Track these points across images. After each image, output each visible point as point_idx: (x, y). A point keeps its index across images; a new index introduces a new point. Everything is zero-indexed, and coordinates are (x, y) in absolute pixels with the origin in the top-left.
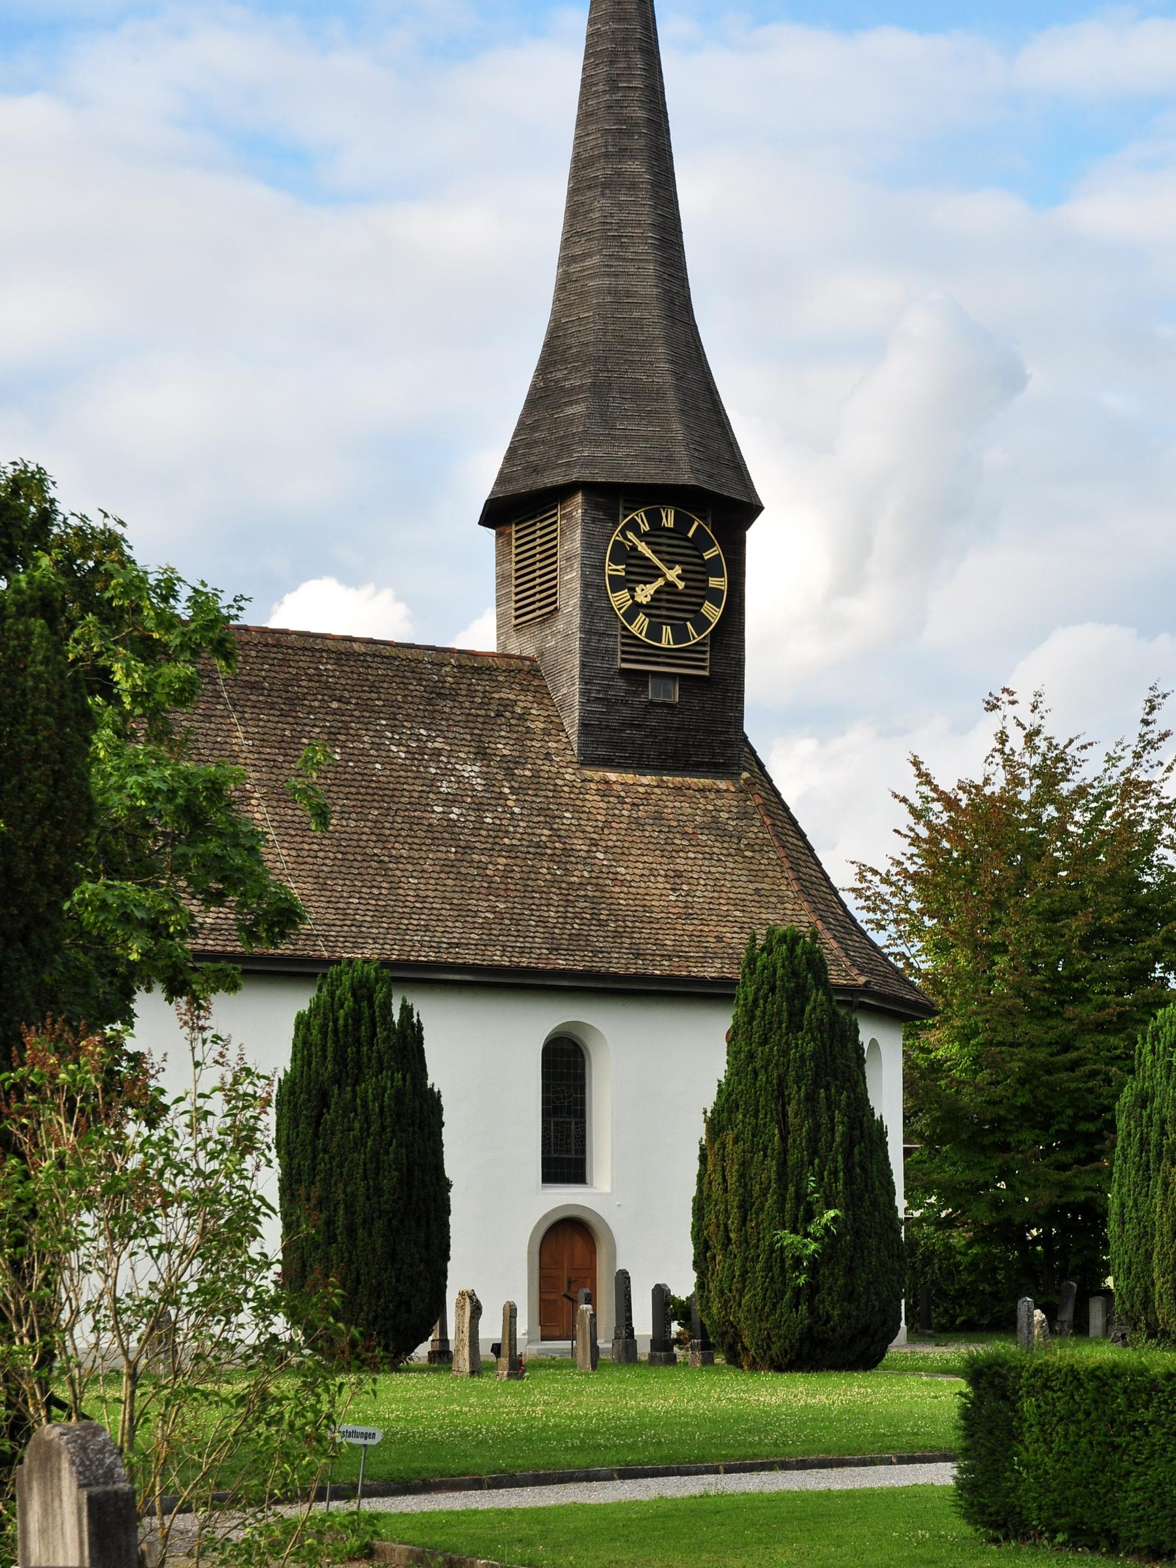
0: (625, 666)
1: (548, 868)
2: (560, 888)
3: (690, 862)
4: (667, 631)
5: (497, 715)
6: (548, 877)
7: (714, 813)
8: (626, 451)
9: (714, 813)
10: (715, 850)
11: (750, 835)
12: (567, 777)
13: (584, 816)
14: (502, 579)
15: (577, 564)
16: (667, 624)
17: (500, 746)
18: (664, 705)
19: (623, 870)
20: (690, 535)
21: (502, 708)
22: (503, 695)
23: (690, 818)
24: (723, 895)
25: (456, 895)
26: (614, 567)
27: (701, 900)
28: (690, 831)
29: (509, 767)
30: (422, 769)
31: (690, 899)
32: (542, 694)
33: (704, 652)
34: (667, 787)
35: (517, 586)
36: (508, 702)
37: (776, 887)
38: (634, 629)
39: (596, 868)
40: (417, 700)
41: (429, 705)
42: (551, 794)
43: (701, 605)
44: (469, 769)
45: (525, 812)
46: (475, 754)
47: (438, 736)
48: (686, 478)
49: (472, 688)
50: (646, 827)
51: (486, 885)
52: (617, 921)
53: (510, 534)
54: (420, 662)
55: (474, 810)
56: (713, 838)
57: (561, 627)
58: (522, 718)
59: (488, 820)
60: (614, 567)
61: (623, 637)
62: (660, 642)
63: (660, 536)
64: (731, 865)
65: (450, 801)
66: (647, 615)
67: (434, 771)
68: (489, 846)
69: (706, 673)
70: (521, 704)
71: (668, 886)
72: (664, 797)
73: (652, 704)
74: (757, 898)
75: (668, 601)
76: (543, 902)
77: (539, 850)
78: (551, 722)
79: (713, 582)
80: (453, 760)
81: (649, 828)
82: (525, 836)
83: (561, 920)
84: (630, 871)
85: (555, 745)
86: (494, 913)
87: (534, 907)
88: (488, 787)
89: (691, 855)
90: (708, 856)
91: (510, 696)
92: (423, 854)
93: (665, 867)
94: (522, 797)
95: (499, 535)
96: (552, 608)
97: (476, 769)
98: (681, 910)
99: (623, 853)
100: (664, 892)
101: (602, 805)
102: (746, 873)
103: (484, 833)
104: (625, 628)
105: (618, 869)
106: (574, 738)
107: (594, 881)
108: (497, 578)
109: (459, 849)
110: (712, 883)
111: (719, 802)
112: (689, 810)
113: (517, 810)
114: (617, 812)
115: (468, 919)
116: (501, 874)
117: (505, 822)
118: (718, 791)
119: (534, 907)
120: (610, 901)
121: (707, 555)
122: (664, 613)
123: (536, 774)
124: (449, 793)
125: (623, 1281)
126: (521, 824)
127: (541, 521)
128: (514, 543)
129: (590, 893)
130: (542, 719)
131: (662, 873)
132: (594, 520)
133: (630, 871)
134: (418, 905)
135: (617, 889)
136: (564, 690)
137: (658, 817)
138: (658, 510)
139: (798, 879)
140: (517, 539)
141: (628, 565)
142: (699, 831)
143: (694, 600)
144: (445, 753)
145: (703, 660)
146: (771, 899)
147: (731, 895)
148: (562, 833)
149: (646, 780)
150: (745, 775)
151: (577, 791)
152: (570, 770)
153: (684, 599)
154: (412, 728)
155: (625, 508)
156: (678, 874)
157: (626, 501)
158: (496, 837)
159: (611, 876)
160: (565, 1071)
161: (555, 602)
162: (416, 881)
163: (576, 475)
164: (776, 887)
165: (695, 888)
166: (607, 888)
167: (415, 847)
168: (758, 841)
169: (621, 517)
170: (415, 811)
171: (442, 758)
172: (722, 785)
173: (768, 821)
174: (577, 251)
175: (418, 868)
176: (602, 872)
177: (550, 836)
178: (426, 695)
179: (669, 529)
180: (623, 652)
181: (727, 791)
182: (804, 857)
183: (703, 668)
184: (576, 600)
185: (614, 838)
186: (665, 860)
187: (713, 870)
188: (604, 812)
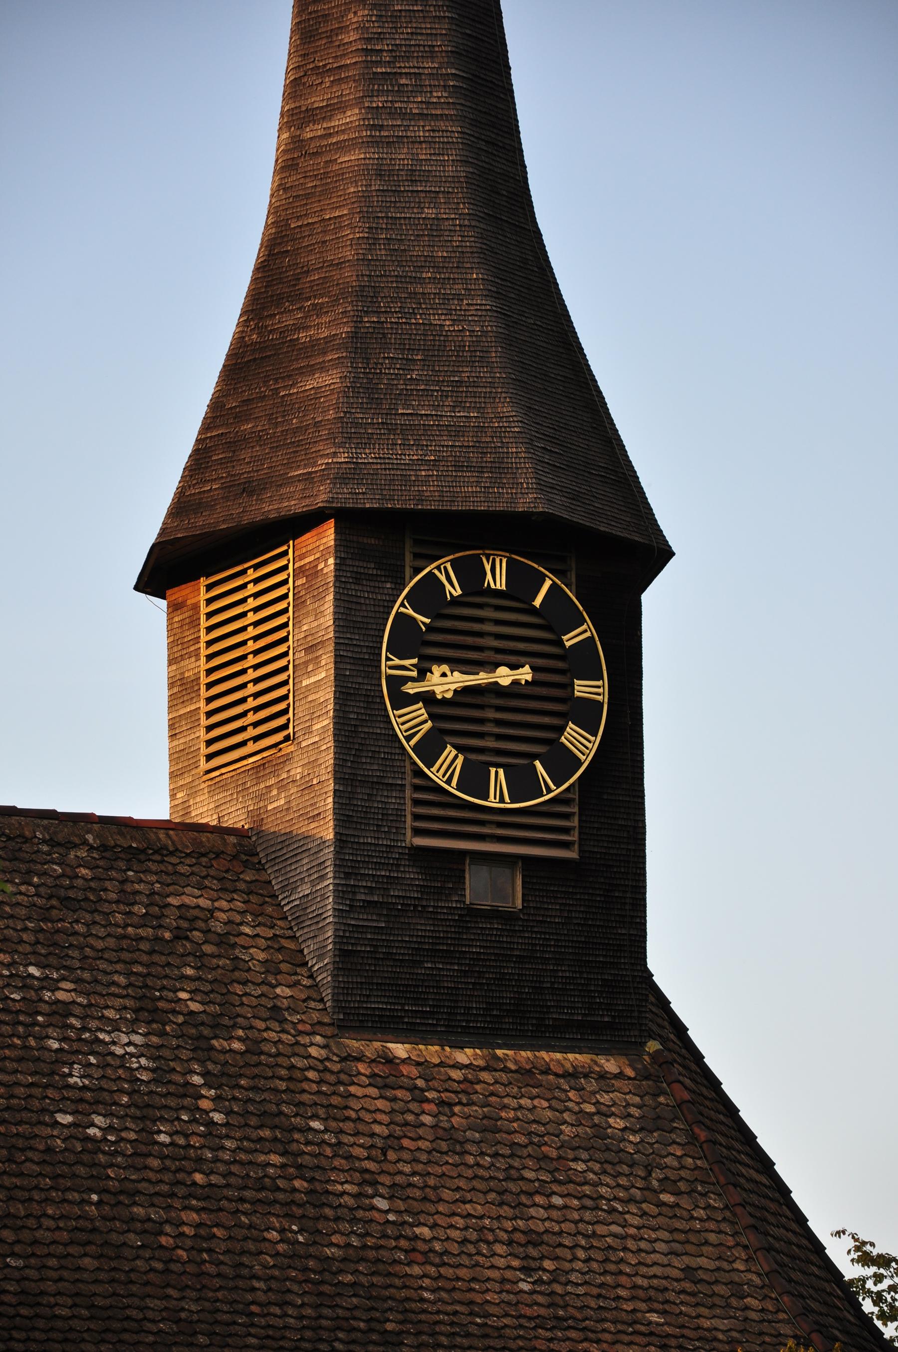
0: (420, 841)
1: (282, 1231)
2: (306, 1269)
3: (555, 1214)
4: (498, 778)
5: (177, 938)
6: (281, 1247)
7: (596, 1119)
8: (415, 455)
9: (596, 1119)
10: (603, 1190)
11: (668, 1160)
12: (313, 1051)
13: (348, 1126)
14: (181, 689)
15: (327, 659)
16: (497, 765)
17: (183, 995)
18: (494, 914)
19: (425, 1232)
20: (537, 602)
21: (184, 924)
22: (187, 900)
23: (551, 1128)
24: (623, 1280)
25: (98, 1289)
26: (397, 662)
27: (581, 1290)
28: (554, 1154)
29: (200, 1036)
30: (32, 1042)
31: (559, 1289)
32: (263, 899)
33: (567, 816)
34: (506, 1070)
35: (209, 700)
36: (196, 912)
37: (725, 1265)
38: (436, 774)
39: (374, 1228)
40: (23, 912)
41: (45, 920)
42: (283, 1085)
43: (561, 730)
44: (125, 1039)
45: (234, 1120)
46: (136, 1011)
47: (64, 979)
48: (526, 498)
49: (128, 887)
50: (468, 1147)
51: (159, 1266)
52: (419, 1333)
53: (196, 607)
54: (26, 840)
55: (134, 1118)
56: (597, 1167)
57: (297, 772)
58: (223, 941)
59: (163, 1138)
60: (397, 662)
62: (486, 798)
63: (480, 606)
64: (636, 1221)
65: (84, 1103)
66: (459, 748)
67: (55, 1045)
68: (165, 1188)
70: (223, 916)
71: (516, 1263)
72: (500, 1089)
73: (473, 912)
74: (688, 1286)
75: (499, 723)
76: (272, 1296)
77: (262, 1195)
78: (280, 949)
79: (582, 688)
80: (93, 1024)
81: (473, 1149)
82: (235, 1169)
83: (308, 1334)
84: (441, 1234)
85: (288, 992)
86: (178, 1321)
87: (254, 1308)
88: (160, 1074)
89: (557, 1201)
90: (589, 1203)
91: (203, 902)
92: (35, 1208)
93: (508, 1225)
94: (227, 1092)
95: (174, 608)
96: (279, 737)
97: (138, 1039)
98: (543, 1311)
99: (425, 1199)
100: (509, 1274)
101: (380, 1104)
102: (665, 1235)
103: (155, 1163)
104: (420, 773)
105: (417, 1230)
106: (324, 978)
107: (372, 1254)
108: (171, 685)
109: (106, 1197)
110: (599, 1256)
111: (605, 1098)
112: (549, 1114)
113: (217, 1117)
114: (410, 1118)
115: (126, 1336)
116: (189, 1243)
117: (195, 1141)
118: (603, 1076)
119: (254, 1308)
120: (403, 1293)
121: (570, 640)
122: (491, 743)
123: (254, 1047)
124: (85, 1088)
126: (228, 1144)
127: (256, 567)
128: (204, 623)
129: (363, 1280)
130: (262, 943)
131: (504, 1236)
132: (358, 578)
133: (441, 1234)
134: (24, 1311)
135: (417, 1270)
136: (305, 890)
137: (490, 1127)
139: (769, 1249)
140: (209, 615)
141: (422, 658)
142: (571, 1155)
143: (546, 720)
144: (77, 1011)
145: (566, 830)
146: (717, 1289)
147: (639, 1281)
148: (306, 1160)
149: (463, 1056)
150: (653, 1046)
151: (332, 1079)
152: (318, 1039)
153: (521, 646)
154: (13, 963)
155: (416, 556)
156: (534, 1239)
157: (416, 542)
158: (179, 1170)
159: (403, 1243)
161: (285, 727)
162: (20, 1263)
163: (323, 497)
164: (725, 1265)
165: (567, 1266)
166: (397, 1268)
167: (19, 1194)
168: (683, 1173)
169: (408, 571)
170: (20, 1123)
171: (73, 1021)
172: (611, 1065)
173: (703, 1135)
174: (317, 101)
175: (26, 1235)
176: (385, 1236)
177: (283, 1166)
178: (39, 901)
179: (497, 593)
180: (416, 817)
181: (620, 1076)
182: (773, 1206)
183: (566, 845)
184: (325, 722)
185: (407, 1169)
186: (506, 1211)
187: (601, 1229)
188: (385, 1118)
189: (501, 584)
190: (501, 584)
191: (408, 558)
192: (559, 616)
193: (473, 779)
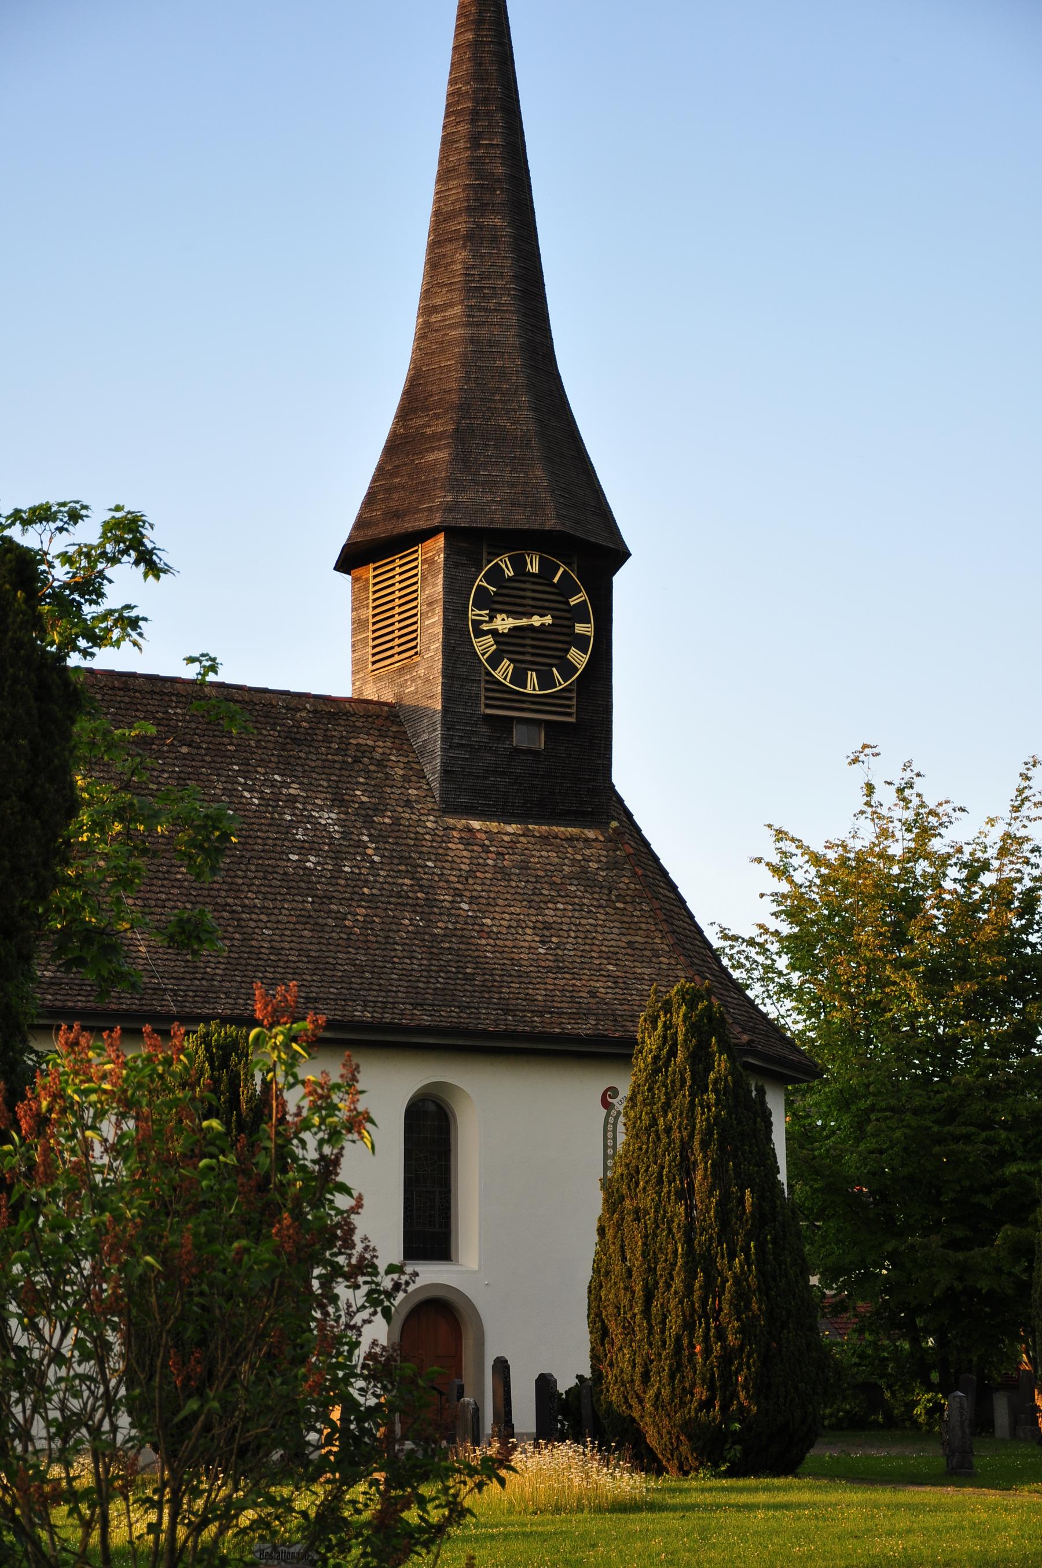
4: (532, 677)
20: (556, 580)
22: (361, 741)
38: (498, 674)
43: (567, 651)
61: (487, 682)
65: (304, 849)
66: (511, 660)
69: (573, 720)
79: (579, 628)
104: (489, 674)
113: (376, 859)
123: (397, 821)
125: (502, 1367)
132: (457, 565)
137: (524, 866)
138: (523, 556)
143: (560, 645)
149: (511, 828)
155: (489, 554)
156: (547, 926)
160: (430, 1133)
172: (591, 834)
183: (569, 714)
189: (535, 569)
190: (535, 569)
191: (485, 555)
192: (567, 588)
193: (519, 678)
